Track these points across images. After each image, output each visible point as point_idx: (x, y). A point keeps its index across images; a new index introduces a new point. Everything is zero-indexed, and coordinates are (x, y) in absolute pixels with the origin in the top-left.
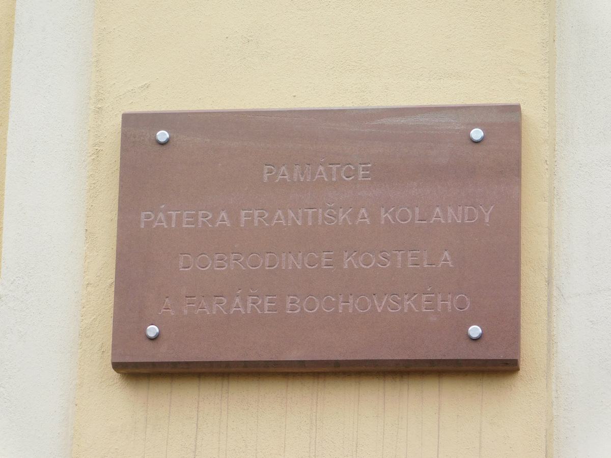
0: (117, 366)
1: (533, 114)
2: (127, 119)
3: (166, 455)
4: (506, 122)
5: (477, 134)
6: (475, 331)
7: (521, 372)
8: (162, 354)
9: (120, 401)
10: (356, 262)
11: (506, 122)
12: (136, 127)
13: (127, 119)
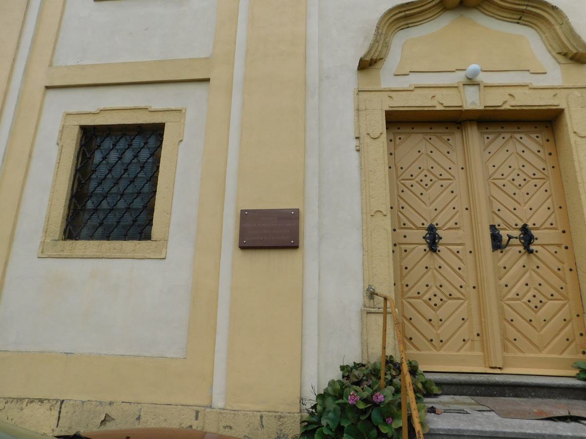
0: (239, 247)
1: (301, 210)
2: (241, 210)
3: (382, 107)
4: (297, 211)
5: (293, 213)
6: (292, 242)
7: (299, 249)
8: (246, 245)
9: (240, 253)
10: (377, 44)
11: (297, 211)
12: (243, 212)
13: (241, 210)
